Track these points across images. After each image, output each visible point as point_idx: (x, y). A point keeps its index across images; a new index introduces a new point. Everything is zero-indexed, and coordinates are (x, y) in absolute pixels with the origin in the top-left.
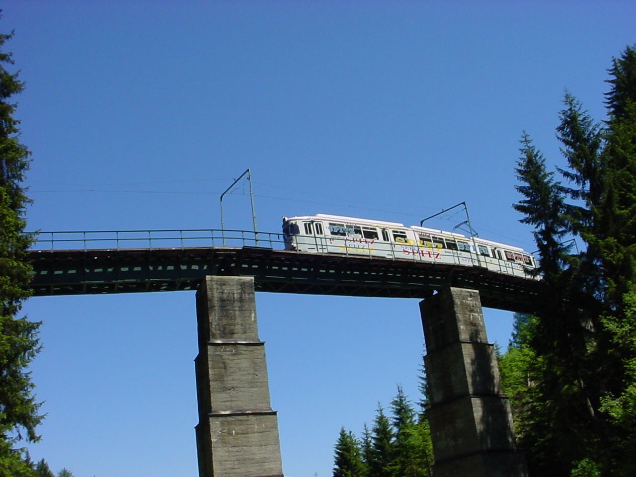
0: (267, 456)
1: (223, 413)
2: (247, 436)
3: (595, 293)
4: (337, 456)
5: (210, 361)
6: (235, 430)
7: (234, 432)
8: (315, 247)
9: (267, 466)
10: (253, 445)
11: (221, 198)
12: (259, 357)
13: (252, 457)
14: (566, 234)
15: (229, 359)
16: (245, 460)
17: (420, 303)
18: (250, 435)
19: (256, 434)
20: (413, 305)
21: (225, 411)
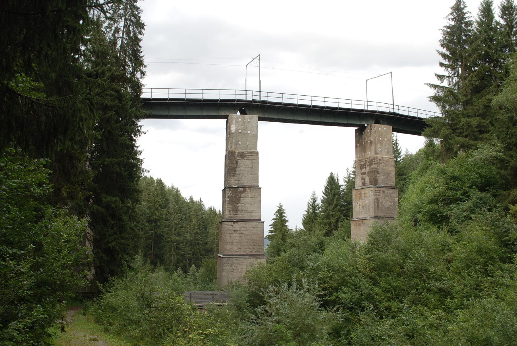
0: (254, 209)
1: (234, 186)
2: (244, 199)
3: (82, 65)
4: (304, 218)
5: (321, 120)
6: (239, 195)
7: (238, 196)
8: (244, 92)
9: (253, 214)
10: (247, 204)
11: (246, 66)
12: (255, 159)
13: (246, 209)
14: (155, 178)
15: (239, 160)
16: (242, 210)
17: (356, 130)
18: (246, 199)
19: (249, 198)
20: (351, 131)
21: (235, 185)
